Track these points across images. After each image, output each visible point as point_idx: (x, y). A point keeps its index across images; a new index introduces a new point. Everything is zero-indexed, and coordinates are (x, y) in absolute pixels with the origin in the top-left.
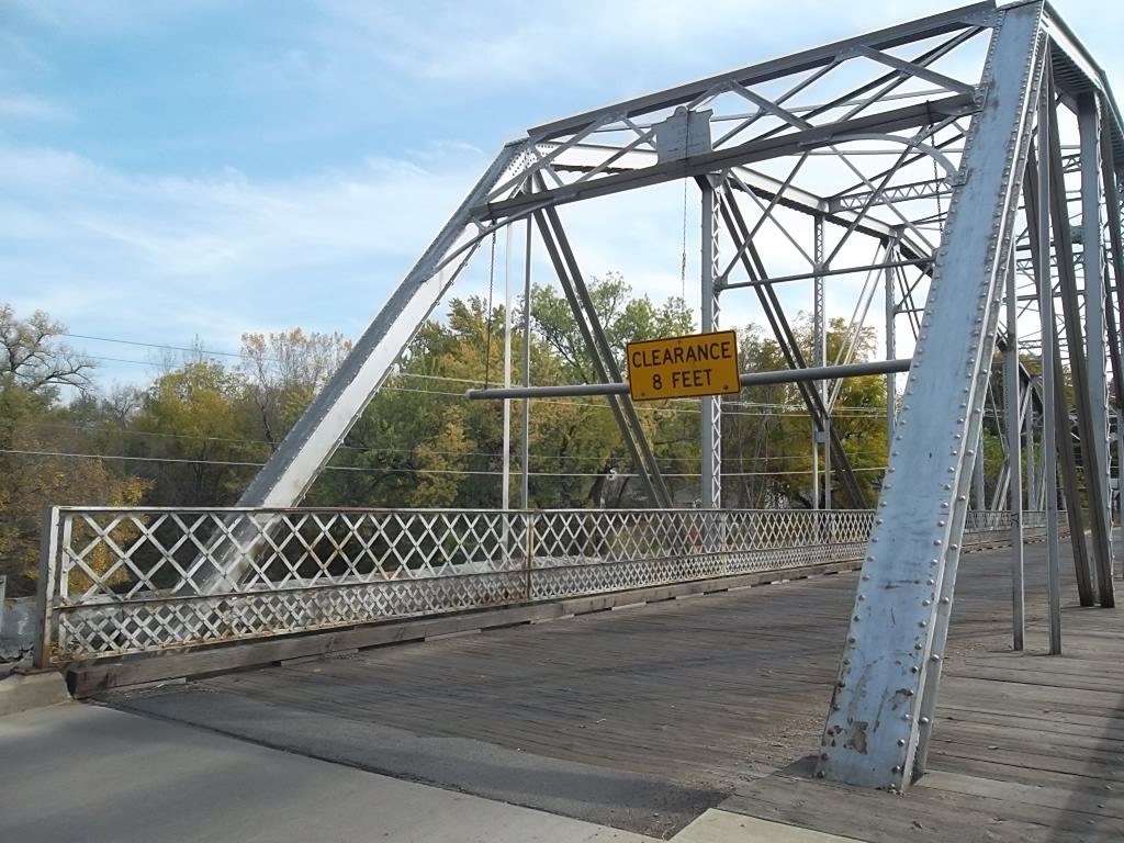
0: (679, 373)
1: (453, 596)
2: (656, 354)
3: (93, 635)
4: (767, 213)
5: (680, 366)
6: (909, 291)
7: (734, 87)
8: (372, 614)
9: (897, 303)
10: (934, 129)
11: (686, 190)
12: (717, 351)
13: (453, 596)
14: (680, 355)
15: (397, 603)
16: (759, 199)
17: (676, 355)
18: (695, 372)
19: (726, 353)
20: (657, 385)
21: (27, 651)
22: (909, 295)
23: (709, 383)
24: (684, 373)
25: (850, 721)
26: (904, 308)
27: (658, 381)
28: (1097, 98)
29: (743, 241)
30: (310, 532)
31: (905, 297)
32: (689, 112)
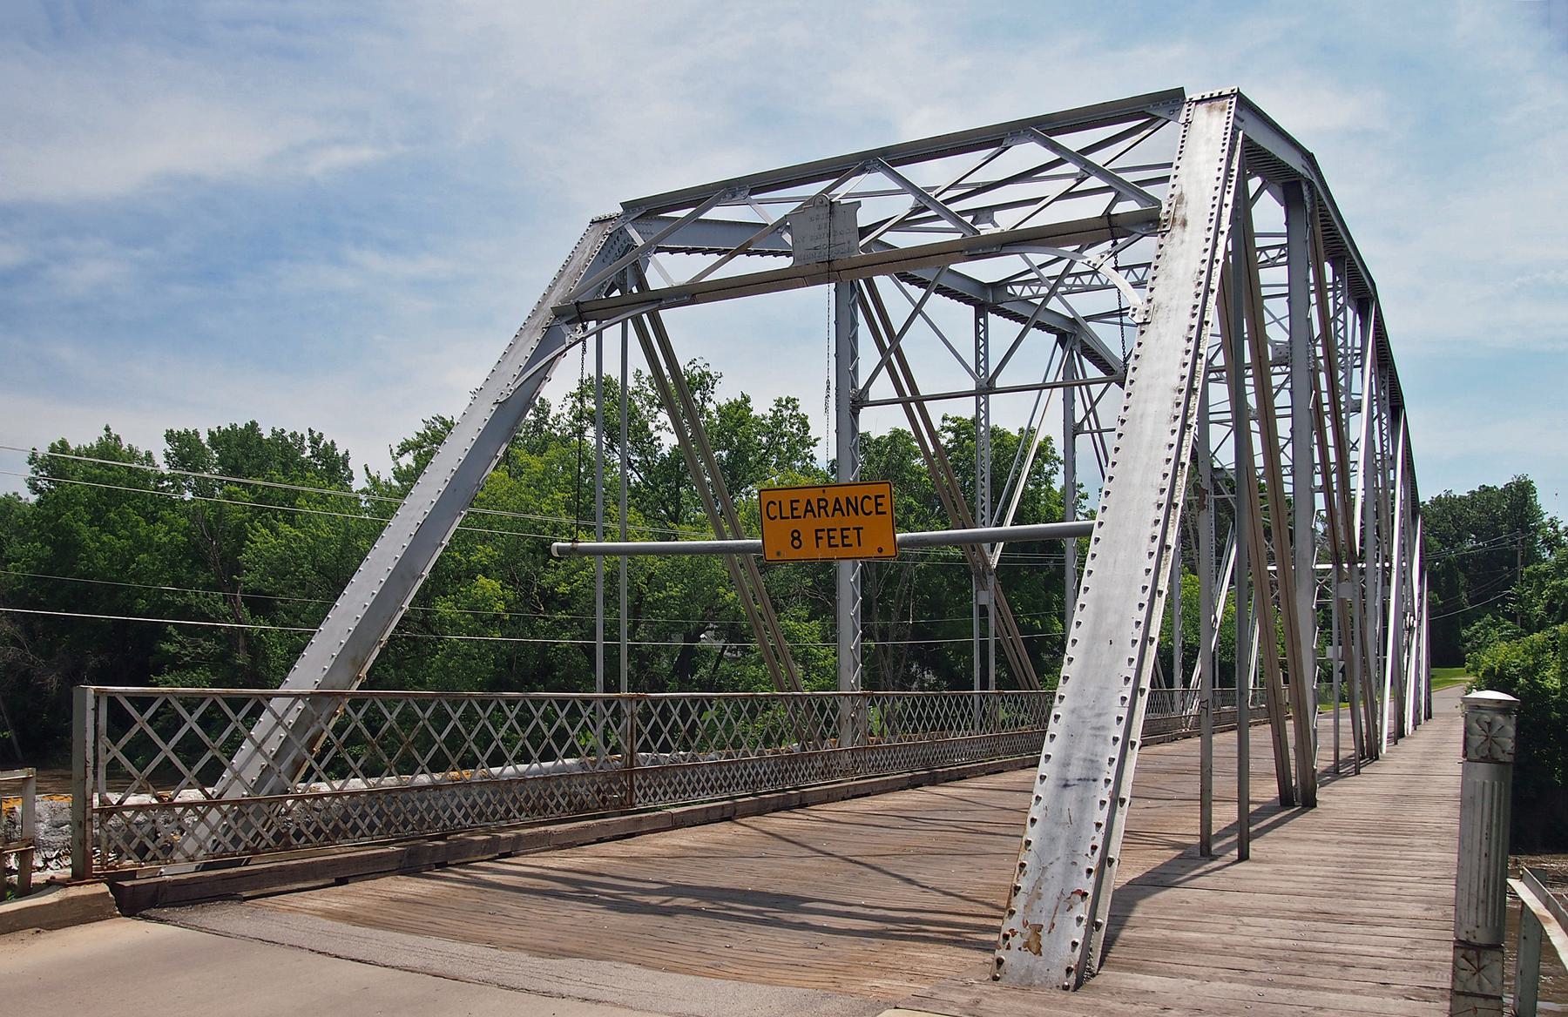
0: (823, 530)
1: (542, 801)
2: (795, 505)
3: (136, 841)
4: (918, 309)
5: (825, 522)
6: (1094, 404)
7: (883, 168)
8: (448, 823)
9: (1078, 421)
10: (1117, 248)
11: (822, 296)
12: (869, 505)
13: (542, 801)
14: (824, 508)
15: (476, 810)
16: (905, 285)
17: (819, 508)
18: (842, 530)
19: (880, 509)
20: (796, 543)
21: (52, 859)
22: (1093, 410)
23: (860, 545)
24: (829, 530)
25: (1025, 924)
26: (1086, 428)
27: (798, 538)
28: (1305, 188)
29: (888, 345)
30: (373, 721)
31: (1088, 413)
32: (831, 203)
